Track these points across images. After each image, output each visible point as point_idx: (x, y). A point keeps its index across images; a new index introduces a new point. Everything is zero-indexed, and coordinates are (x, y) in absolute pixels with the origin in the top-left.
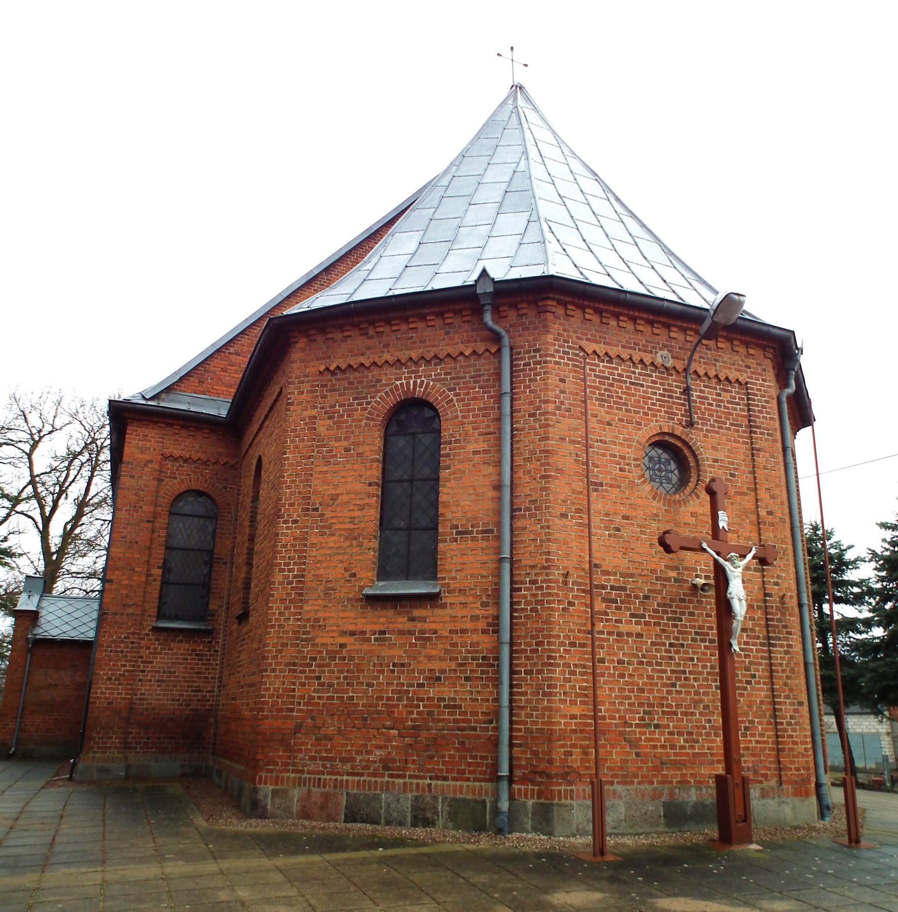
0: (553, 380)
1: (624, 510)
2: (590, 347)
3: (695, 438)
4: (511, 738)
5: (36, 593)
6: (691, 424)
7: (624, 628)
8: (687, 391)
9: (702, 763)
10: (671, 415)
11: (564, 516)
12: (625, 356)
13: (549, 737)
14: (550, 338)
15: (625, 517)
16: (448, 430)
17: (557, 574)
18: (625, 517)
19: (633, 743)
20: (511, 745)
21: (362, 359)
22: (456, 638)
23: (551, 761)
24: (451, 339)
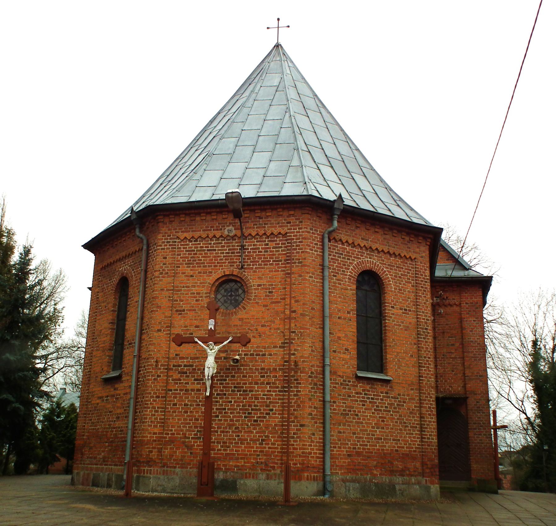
0: (159, 259)
1: (197, 323)
2: (182, 236)
4: (132, 444)
7: (189, 387)
8: (243, 247)
10: (232, 263)
11: (159, 330)
12: (204, 236)
14: (160, 236)
15: (197, 327)
18: (197, 327)
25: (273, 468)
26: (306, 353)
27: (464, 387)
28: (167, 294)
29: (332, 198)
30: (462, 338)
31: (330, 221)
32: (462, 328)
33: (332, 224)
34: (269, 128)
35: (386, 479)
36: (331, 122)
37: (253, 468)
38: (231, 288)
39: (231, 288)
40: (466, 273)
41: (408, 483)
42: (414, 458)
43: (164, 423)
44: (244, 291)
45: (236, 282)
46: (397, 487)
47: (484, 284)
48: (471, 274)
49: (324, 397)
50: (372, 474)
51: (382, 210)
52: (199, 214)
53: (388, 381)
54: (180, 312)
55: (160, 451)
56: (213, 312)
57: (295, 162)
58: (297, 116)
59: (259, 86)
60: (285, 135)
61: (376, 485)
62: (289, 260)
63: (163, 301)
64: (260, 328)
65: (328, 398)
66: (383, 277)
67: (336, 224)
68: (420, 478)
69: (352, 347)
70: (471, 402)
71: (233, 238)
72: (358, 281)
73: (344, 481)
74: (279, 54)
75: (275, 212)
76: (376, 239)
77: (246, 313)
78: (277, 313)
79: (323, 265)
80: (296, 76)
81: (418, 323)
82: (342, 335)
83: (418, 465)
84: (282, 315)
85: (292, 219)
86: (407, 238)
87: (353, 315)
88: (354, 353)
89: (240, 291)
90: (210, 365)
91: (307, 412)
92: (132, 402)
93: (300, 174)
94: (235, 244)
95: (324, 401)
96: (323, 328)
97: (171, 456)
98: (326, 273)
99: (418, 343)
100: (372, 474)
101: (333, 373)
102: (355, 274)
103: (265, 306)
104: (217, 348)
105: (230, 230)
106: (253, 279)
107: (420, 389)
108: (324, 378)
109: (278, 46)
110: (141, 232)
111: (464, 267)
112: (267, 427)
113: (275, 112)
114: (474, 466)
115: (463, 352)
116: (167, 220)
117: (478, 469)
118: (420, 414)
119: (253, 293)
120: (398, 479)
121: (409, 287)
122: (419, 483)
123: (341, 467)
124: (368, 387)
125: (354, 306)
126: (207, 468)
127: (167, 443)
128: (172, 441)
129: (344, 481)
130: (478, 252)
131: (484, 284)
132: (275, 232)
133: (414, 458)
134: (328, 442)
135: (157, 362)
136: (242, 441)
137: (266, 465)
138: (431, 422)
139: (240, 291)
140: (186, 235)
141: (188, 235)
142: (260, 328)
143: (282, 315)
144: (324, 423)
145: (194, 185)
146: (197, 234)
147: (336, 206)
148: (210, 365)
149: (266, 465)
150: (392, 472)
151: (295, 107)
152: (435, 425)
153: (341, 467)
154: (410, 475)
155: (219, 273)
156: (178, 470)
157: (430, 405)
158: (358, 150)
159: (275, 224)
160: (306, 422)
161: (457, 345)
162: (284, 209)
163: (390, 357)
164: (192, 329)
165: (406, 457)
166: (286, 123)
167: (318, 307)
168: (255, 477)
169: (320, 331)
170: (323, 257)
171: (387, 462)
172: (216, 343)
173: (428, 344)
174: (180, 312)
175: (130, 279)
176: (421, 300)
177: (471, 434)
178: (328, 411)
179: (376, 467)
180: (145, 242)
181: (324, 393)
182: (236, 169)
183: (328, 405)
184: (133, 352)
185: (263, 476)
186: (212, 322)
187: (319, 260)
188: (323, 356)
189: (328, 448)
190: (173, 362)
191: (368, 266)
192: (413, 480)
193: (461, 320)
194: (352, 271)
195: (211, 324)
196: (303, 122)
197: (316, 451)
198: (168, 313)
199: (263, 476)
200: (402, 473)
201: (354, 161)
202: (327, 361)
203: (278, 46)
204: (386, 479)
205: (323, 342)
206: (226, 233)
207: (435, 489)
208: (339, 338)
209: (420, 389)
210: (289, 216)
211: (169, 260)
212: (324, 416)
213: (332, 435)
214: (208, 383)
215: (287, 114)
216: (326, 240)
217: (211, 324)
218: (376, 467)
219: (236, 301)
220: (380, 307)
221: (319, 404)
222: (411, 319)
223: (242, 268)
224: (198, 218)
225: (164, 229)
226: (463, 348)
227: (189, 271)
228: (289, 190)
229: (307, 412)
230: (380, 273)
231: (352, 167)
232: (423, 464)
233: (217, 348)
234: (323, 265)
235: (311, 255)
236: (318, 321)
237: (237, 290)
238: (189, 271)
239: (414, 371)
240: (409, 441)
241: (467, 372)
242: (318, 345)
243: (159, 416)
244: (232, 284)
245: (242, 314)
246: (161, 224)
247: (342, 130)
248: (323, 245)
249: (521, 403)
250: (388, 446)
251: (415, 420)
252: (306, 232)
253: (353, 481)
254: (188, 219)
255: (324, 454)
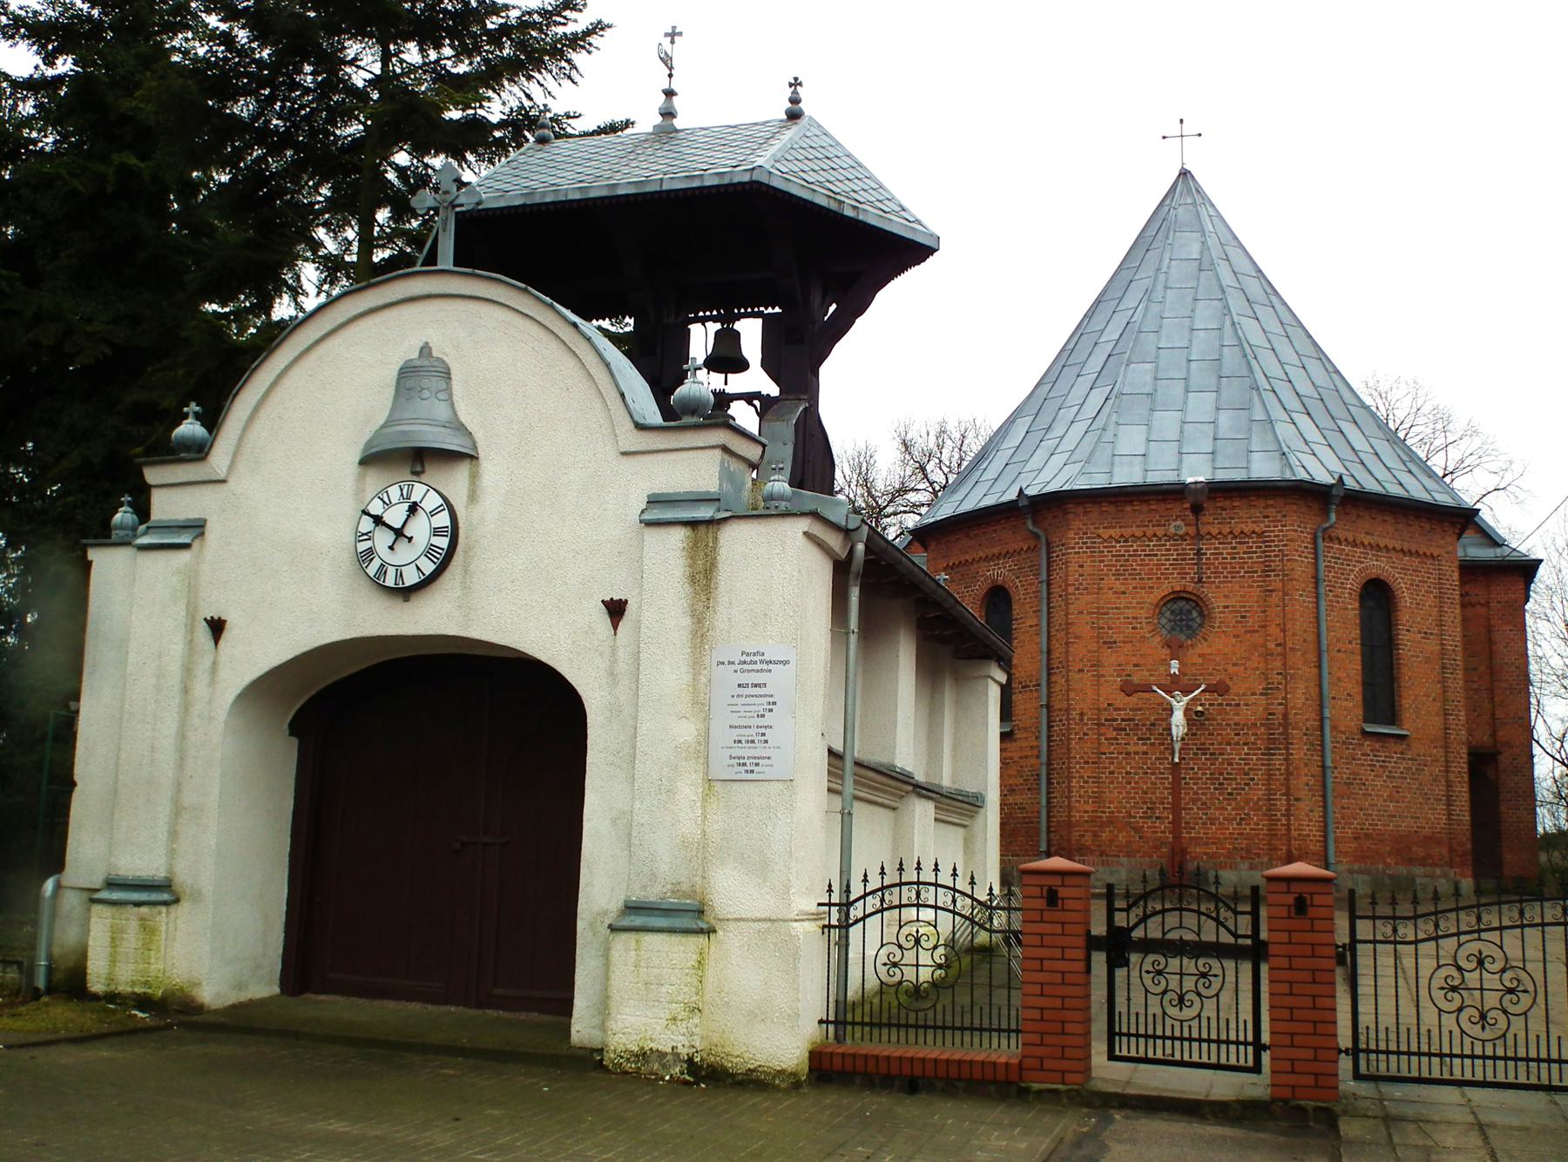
0: (1073, 567)
1: (1135, 660)
2: (1106, 534)
3: (1207, 592)
4: (1048, 827)
5: (1341, 909)
6: (1200, 581)
7: (1131, 749)
8: (1199, 553)
9: (1197, 844)
10: (1183, 574)
11: (1081, 671)
12: (1139, 533)
13: (1069, 825)
14: (1071, 534)
15: (1136, 665)
16: (1016, 610)
17: (1075, 714)
18: (1136, 665)
19: (1137, 830)
20: (1049, 832)
21: (967, 557)
22: (1022, 762)
23: (1069, 841)
24: (1008, 537)
25: (1258, 855)
26: (1299, 703)
27: (1494, 734)
28: (1088, 618)
29: (1327, 479)
30: (1491, 658)
31: (1325, 512)
32: (1491, 642)
33: (1328, 518)
34: (1202, 344)
35: (1402, 870)
36: (1292, 324)
37: (1229, 854)
38: (1185, 612)
39: (1185, 612)
40: (1499, 551)
41: (1432, 876)
42: (1439, 842)
43: (1098, 798)
44: (1201, 614)
45: (1187, 600)
46: (1418, 881)
47: (1527, 569)
48: (1507, 551)
49: (1323, 761)
50: (1385, 863)
51: (1394, 490)
52: (1131, 502)
53: (1404, 737)
54: (1110, 644)
55: (1095, 835)
56: (1175, 649)
57: (1259, 414)
58: (1244, 320)
59: (1167, 261)
60: (1231, 359)
61: (1391, 876)
62: (1267, 571)
63: (1083, 627)
64: (1230, 667)
65: (1329, 763)
66: (1395, 586)
67: (1333, 517)
68: (1447, 869)
69: (1355, 689)
70: (1504, 760)
71: (1183, 538)
72: (1361, 596)
73: (1351, 872)
74: (1189, 191)
75: (1245, 501)
76: (1384, 532)
77: (1209, 646)
78: (1254, 647)
79: (1316, 577)
80: (1226, 237)
81: (1443, 652)
82: (1342, 674)
83: (1444, 851)
84: (1262, 650)
85: (1271, 512)
86: (1427, 526)
87: (1356, 646)
88: (1359, 698)
89: (1195, 614)
90: (1178, 720)
91: (1304, 781)
92: (1044, 768)
93: (1270, 437)
94: (1186, 546)
95: (1324, 767)
96: (1319, 667)
97: (1111, 841)
98: (1322, 590)
99: (1443, 681)
100: (1385, 863)
101: (1334, 728)
102: (1357, 587)
103: (1236, 636)
104: (1186, 699)
105: (1176, 526)
106: (1217, 599)
107: (1446, 746)
108: (1322, 735)
109: (1184, 174)
110: (1035, 523)
111: (1489, 538)
112: (1247, 802)
113: (1206, 315)
114: (1508, 857)
115: (1492, 681)
116: (1080, 510)
117: (1512, 861)
118: (1447, 781)
119: (1218, 616)
120: (1419, 870)
121: (1431, 600)
122: (1445, 876)
123: (1346, 854)
124: (1377, 746)
125: (1356, 632)
126: (1178, 853)
127: (1103, 825)
128: (1111, 821)
129: (1351, 872)
130: (1477, 442)
131: (1527, 569)
132: (1246, 530)
133: (1439, 842)
134: (1330, 822)
135: (1082, 714)
136: (1213, 821)
137: (1248, 851)
138: (1462, 792)
139: (1195, 614)
140: (1111, 532)
141: (1115, 532)
142: (1230, 667)
143: (1262, 650)
144: (1324, 796)
145: (1109, 451)
146: (1127, 532)
147: (1334, 492)
148: (1178, 720)
149: (1248, 851)
150: (1410, 861)
151: (1236, 303)
152: (1466, 796)
153: (1346, 854)
154: (1434, 865)
155: (1165, 588)
156: (1123, 860)
157: (1461, 767)
158: (1337, 372)
159: (1246, 518)
160: (1302, 794)
161: (1482, 668)
162: (1258, 497)
163: (1407, 702)
164: (1130, 668)
165: (1430, 840)
166: (1229, 340)
167: (1311, 638)
168: (1233, 866)
169: (1315, 671)
170: (1316, 565)
171: (1403, 847)
172: (1186, 692)
173: (1457, 682)
174: (1110, 644)
175: (1012, 591)
176: (1448, 619)
177: (1503, 808)
178: (1330, 781)
179: (1390, 854)
180: (1043, 539)
181: (1323, 756)
182: (1167, 423)
183: (1329, 772)
184: (1039, 698)
185: (1245, 866)
186: (1175, 664)
187: (1311, 570)
188: (1321, 706)
189: (1331, 827)
190: (1105, 715)
191: (1374, 573)
192: (1438, 871)
193: (1489, 629)
194: (1353, 583)
195: (1175, 667)
196: (1256, 338)
197: (1316, 833)
198: (1094, 647)
199: (1245, 866)
200: (1423, 862)
201: (1336, 401)
202: (1327, 713)
203: (1184, 174)
204: (1402, 870)
205: (1320, 686)
206: (1172, 530)
207: (1467, 884)
208: (1339, 679)
209: (1446, 746)
210: (1267, 507)
211: (1087, 570)
212: (1324, 786)
213: (1334, 812)
214: (1177, 746)
215: (1228, 323)
216: (1320, 541)
217: (1175, 667)
218: (1390, 854)
219: (1189, 627)
220: (1390, 630)
221: (1316, 770)
222: (1432, 646)
223: (1200, 581)
224: (1128, 508)
225: (1076, 524)
226: (1491, 674)
227: (1118, 586)
228: (1263, 468)
229: (1304, 781)
230: (1390, 581)
231: (1338, 411)
232: (1451, 850)
233: (1186, 699)
234: (1316, 577)
235: (1301, 564)
236: (1312, 657)
237: (1190, 612)
238: (1118, 586)
239: (1438, 721)
240: (1433, 818)
241: (1498, 713)
242: (1314, 691)
243: (1092, 788)
244: (1181, 604)
245: (1202, 648)
246: (1071, 516)
247: (1310, 336)
248: (1315, 548)
249: (1558, 744)
250: (1406, 825)
251: (1440, 790)
252: (1291, 531)
253: (1361, 872)
254: (1112, 509)
255: (1325, 837)
